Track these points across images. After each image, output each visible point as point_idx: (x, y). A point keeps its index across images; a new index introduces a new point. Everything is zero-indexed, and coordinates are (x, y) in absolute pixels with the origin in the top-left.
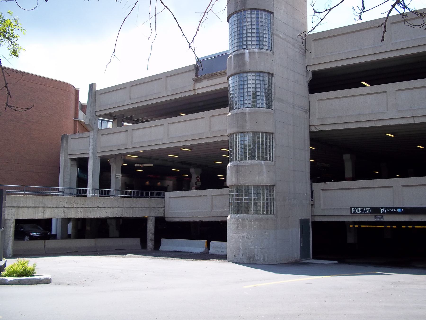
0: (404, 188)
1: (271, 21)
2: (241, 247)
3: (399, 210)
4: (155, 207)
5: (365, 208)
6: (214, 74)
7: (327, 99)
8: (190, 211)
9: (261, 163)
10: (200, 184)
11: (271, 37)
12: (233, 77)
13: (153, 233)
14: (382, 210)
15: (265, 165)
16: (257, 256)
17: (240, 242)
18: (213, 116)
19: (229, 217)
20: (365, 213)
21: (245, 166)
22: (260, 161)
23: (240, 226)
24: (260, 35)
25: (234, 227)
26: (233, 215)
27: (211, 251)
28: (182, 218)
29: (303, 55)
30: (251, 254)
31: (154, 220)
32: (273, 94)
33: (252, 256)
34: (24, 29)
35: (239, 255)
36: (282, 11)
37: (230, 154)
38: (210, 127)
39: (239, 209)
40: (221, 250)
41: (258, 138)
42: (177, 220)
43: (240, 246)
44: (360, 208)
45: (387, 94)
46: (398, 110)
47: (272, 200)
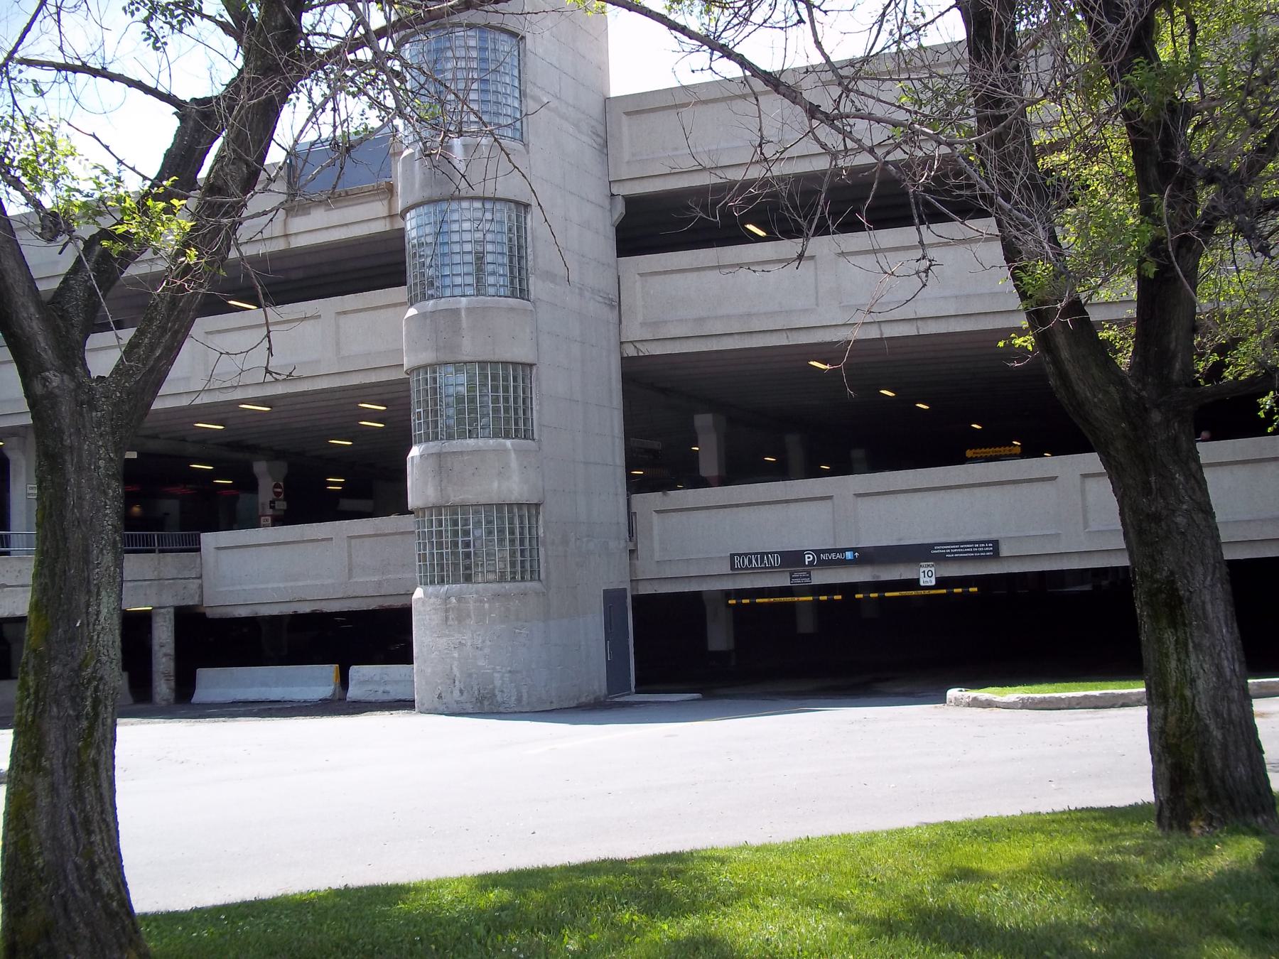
0: (859, 499)
1: (519, 60)
2: (456, 671)
3: (849, 555)
4: (175, 577)
5: (767, 554)
6: (346, 192)
7: (665, 272)
8: (281, 585)
9: (505, 445)
10: (285, 508)
11: (521, 104)
12: (418, 209)
13: (170, 655)
14: (809, 558)
15: (515, 450)
16: (502, 691)
17: (453, 658)
18: (345, 313)
19: (419, 593)
20: (766, 568)
21: (462, 453)
22: (501, 440)
23: (453, 615)
24: (491, 97)
25: (437, 619)
26: (430, 589)
27: (354, 692)
28: (258, 606)
29: (601, 151)
30: (485, 689)
31: (173, 617)
32: (529, 259)
33: (487, 693)
34: (87, 160)
35: (452, 692)
36: (547, 34)
37: (417, 422)
38: (338, 344)
39: (447, 571)
40: (381, 689)
41: (495, 378)
42: (243, 612)
43: (455, 670)
44: (755, 554)
45: (816, 265)
46: (842, 305)
47: (534, 542)
